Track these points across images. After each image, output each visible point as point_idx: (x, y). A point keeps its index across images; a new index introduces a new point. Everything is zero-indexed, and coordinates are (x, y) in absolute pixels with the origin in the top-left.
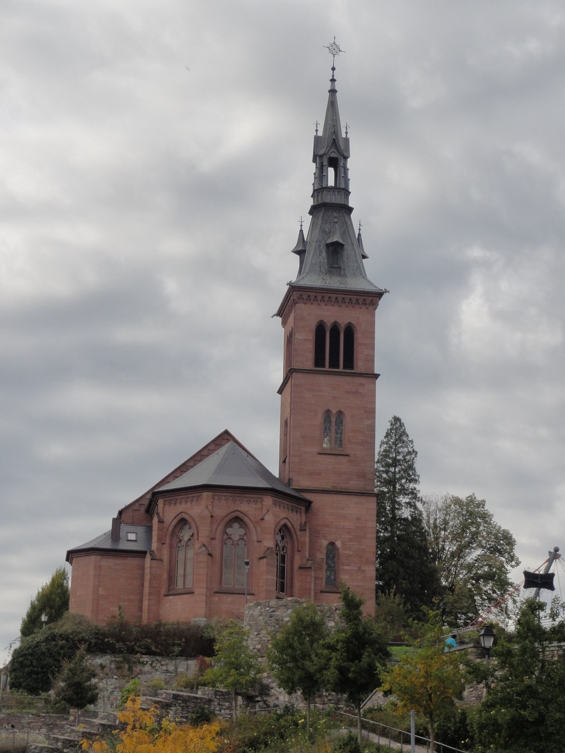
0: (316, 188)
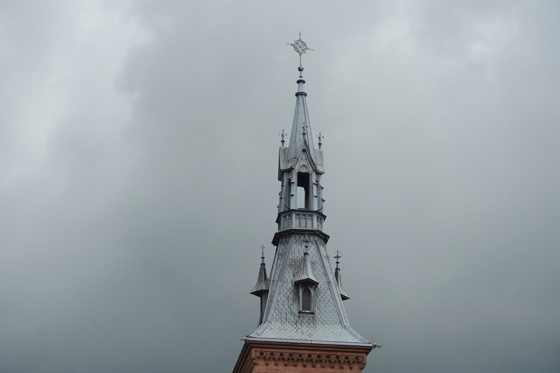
0: (282, 211)
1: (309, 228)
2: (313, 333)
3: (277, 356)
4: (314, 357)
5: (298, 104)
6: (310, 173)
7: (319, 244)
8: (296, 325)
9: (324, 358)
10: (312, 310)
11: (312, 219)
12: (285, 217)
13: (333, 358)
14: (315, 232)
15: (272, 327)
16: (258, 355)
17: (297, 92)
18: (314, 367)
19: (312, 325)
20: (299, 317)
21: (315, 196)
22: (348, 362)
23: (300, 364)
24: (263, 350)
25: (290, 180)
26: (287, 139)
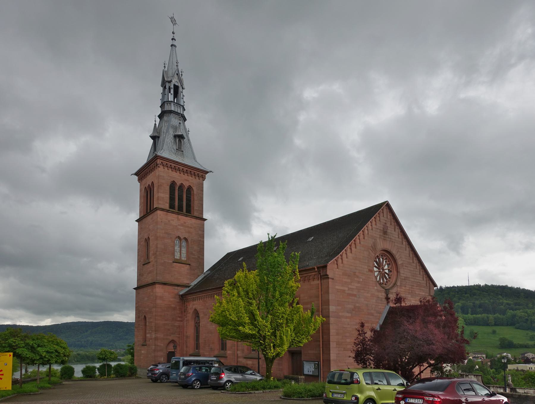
16: (160, 163)
17: (171, 44)
24: (163, 161)
26: (167, 66)
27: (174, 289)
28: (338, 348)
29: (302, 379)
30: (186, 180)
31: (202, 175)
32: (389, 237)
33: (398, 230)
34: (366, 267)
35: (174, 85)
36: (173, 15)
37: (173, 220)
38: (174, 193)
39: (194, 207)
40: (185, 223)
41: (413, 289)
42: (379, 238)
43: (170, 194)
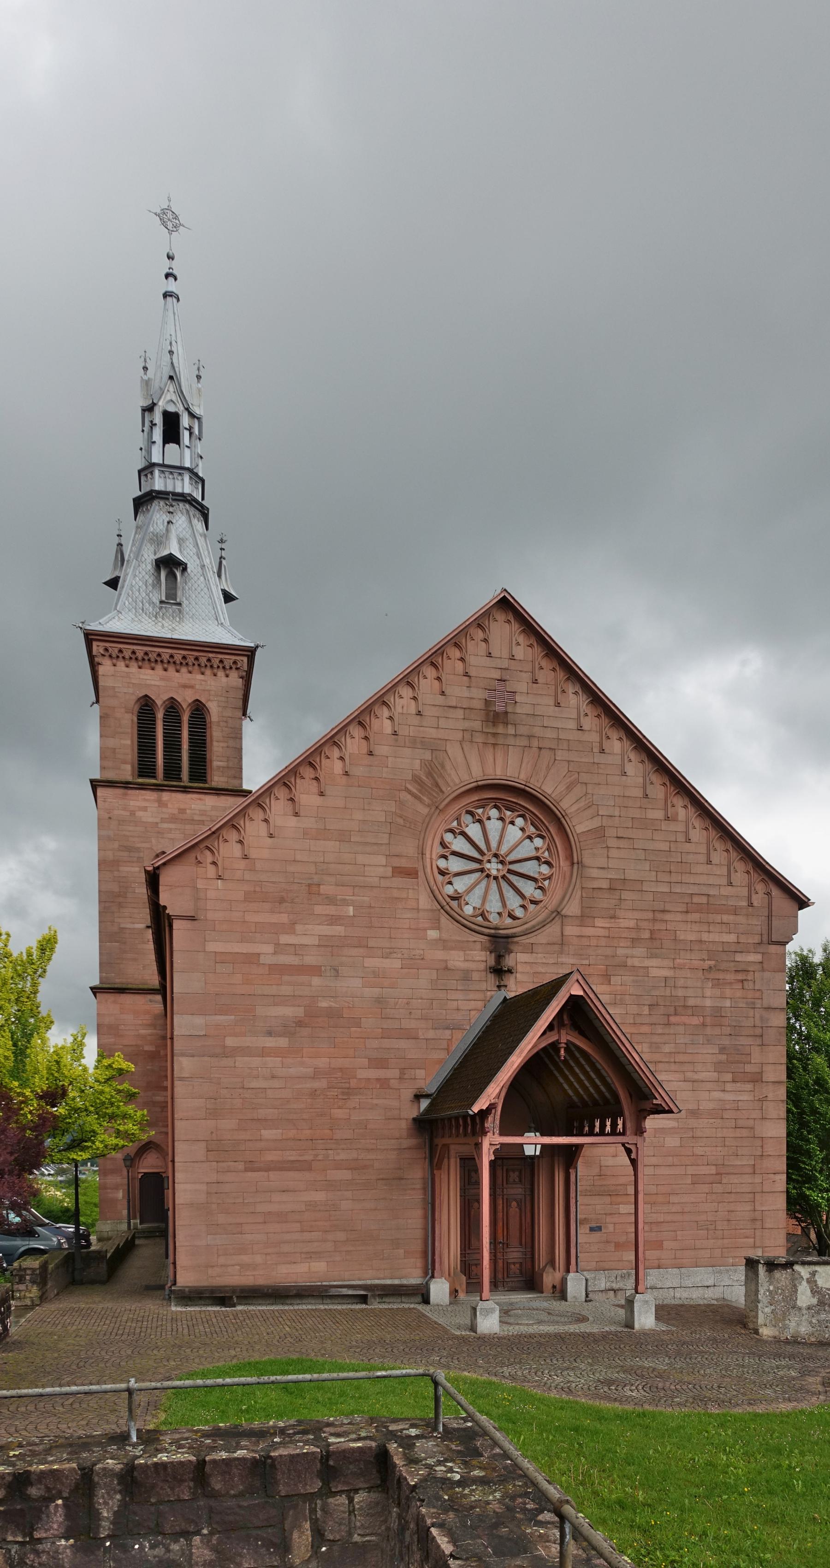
1: (179, 490)
2: (177, 628)
3: (127, 654)
4: (178, 658)
5: (165, 304)
6: (181, 414)
7: (192, 516)
8: (156, 617)
9: (191, 660)
10: (178, 600)
11: (183, 480)
12: (146, 475)
13: (203, 661)
14: (185, 497)
15: (122, 617)
16: (102, 652)
17: (163, 291)
18: (178, 671)
19: (178, 619)
20: (161, 608)
21: (187, 447)
22: (224, 668)
23: (159, 667)
24: (108, 645)
25: (152, 422)
27: (151, 1001)
28: (217, 1162)
29: (28, 1272)
30: (185, 686)
31: (235, 662)
32: (522, 730)
33: (575, 700)
34: (382, 860)
35: (166, 415)
36: (170, 201)
37: (145, 809)
38: (153, 730)
39: (211, 761)
40: (182, 811)
41: (658, 926)
42: (461, 742)
43: (140, 736)
